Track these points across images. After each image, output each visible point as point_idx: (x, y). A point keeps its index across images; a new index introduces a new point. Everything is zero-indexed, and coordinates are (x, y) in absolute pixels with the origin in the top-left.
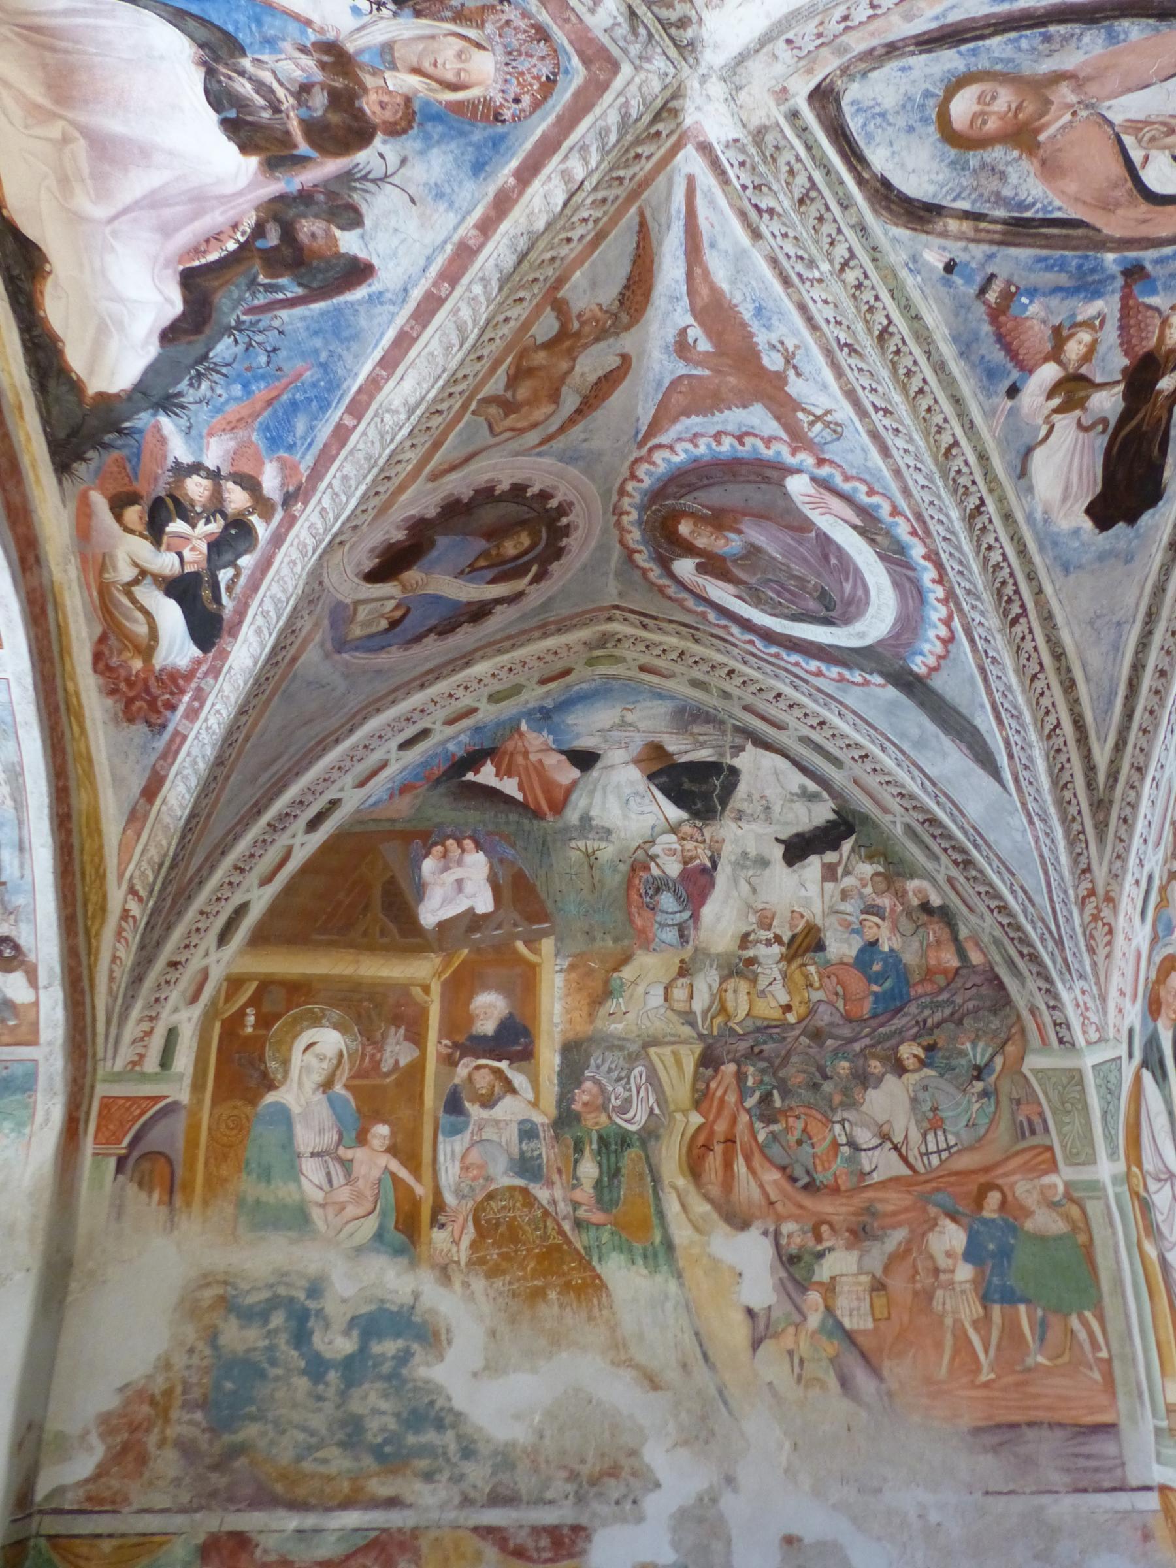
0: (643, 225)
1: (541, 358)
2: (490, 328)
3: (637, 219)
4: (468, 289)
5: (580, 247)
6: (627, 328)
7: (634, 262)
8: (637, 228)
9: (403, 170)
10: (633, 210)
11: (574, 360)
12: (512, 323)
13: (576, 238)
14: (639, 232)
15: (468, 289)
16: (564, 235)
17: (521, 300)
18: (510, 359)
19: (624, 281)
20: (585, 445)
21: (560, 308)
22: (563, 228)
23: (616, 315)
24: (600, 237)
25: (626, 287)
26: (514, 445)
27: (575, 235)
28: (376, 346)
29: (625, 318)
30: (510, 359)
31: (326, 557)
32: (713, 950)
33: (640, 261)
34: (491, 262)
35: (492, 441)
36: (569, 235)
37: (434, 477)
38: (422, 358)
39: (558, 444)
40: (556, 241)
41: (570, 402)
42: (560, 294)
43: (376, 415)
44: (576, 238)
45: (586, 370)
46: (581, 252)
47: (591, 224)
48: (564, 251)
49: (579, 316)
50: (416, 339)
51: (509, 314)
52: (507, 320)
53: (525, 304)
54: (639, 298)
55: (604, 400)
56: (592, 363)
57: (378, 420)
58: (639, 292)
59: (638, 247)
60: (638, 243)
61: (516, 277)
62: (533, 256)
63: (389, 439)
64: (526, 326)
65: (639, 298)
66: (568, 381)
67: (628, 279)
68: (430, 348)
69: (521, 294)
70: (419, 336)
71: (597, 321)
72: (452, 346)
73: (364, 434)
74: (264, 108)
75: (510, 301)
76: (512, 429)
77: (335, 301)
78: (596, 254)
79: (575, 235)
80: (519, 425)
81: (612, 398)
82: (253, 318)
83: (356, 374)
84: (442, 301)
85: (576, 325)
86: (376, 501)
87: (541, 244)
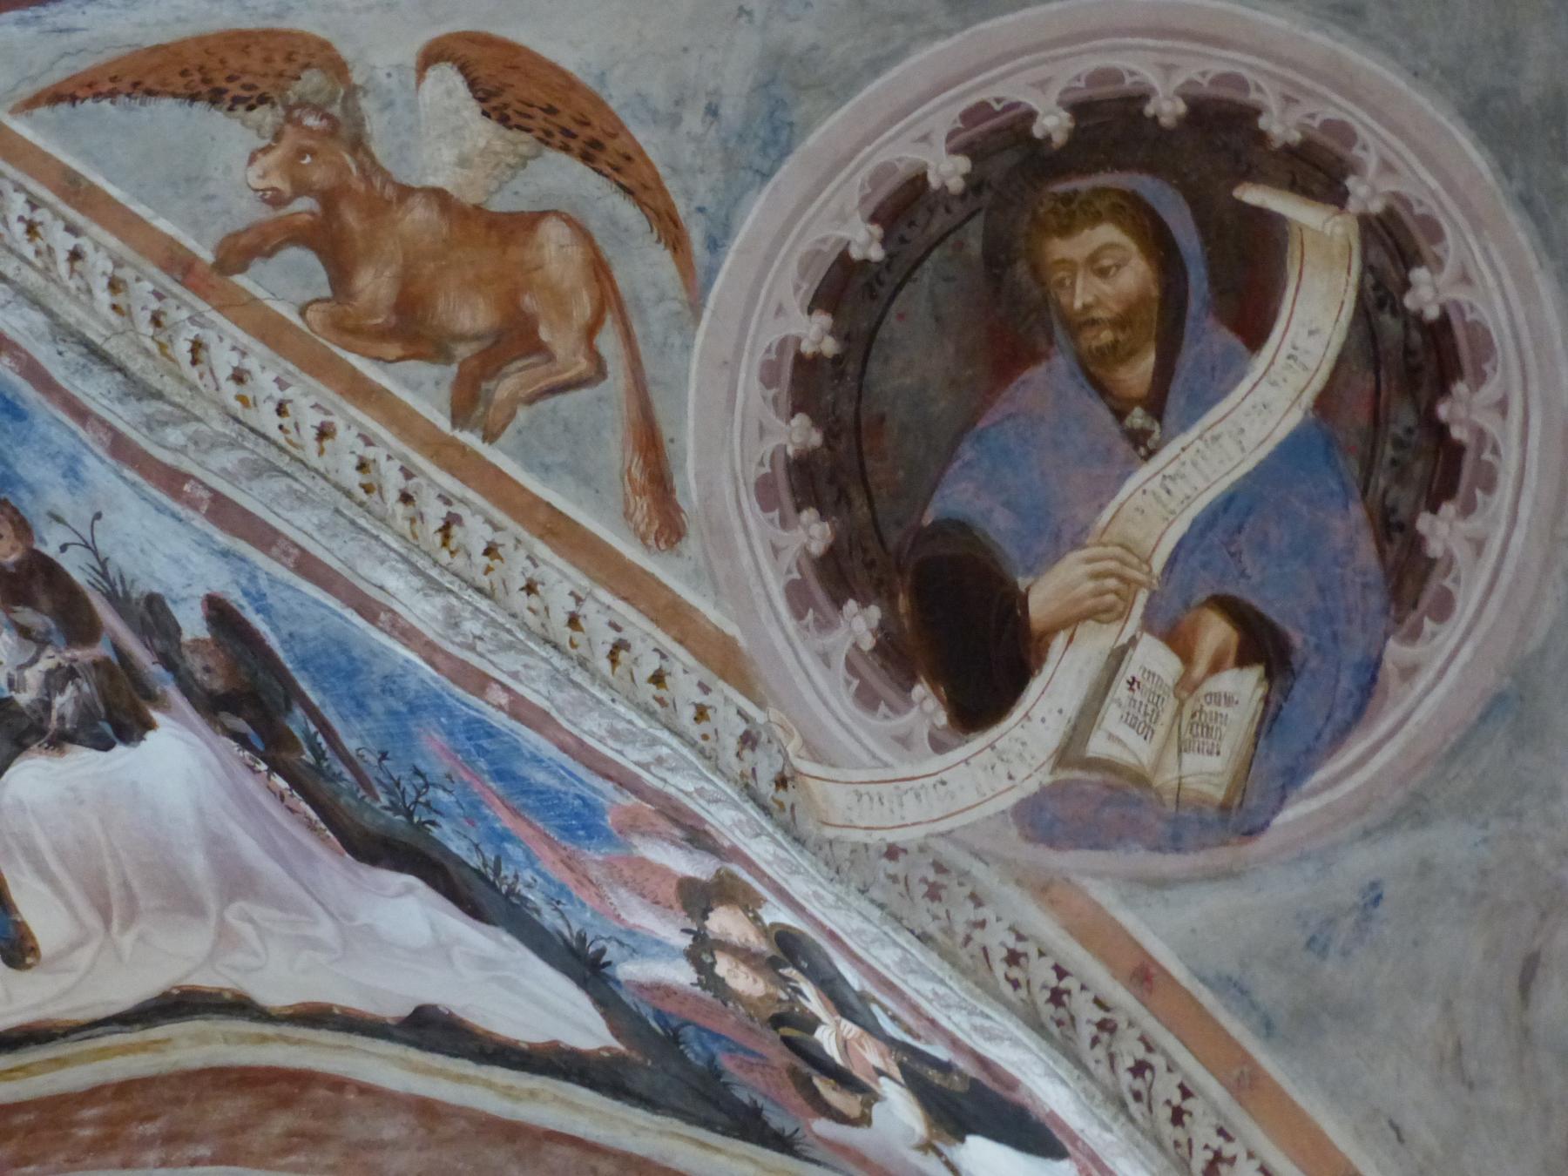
0: (56, 96)
1: (375, 285)
2: (250, 416)
3: (43, 112)
4: (182, 450)
5: (95, 229)
6: (338, 68)
7: (150, 93)
8: (63, 109)
9: (68, 520)
10: (21, 127)
11: (405, 192)
12: (251, 364)
13: (70, 242)
14: (73, 99)
15: (182, 450)
16: (63, 268)
17: (197, 347)
18: (353, 359)
19: (200, 108)
20: (727, 110)
21: (240, 252)
22: (46, 272)
23: (289, 109)
24: (74, 189)
25: (215, 97)
26: (652, 323)
27: (63, 243)
28: (341, 617)
29: (312, 81)
30: (353, 359)
31: (808, 826)
32: (1071, 125)
33: (149, 82)
34: (118, 408)
35: (617, 378)
36: (62, 256)
37: (668, 527)
38: (334, 545)
39: (689, 196)
40: (72, 284)
41: (560, 176)
42: (207, 256)
43: (472, 648)
44: (70, 242)
45: (448, 155)
46: (104, 224)
47: (41, 215)
48: (99, 264)
49: (276, 200)
50: (303, 551)
51: (224, 372)
52: (239, 377)
53: (209, 337)
54: (254, 62)
55: (569, 83)
56: (438, 140)
57: (480, 646)
58: (235, 62)
59: (112, 95)
60: (98, 96)
61: (137, 365)
62: (95, 333)
63: (506, 637)
64: (271, 331)
65: (254, 62)
66: (470, 197)
67: (194, 98)
68: (309, 528)
69: (182, 348)
70: (296, 545)
71: (301, 152)
72: (290, 487)
73: (514, 675)
74: (79, 688)
75: (192, 373)
76: (591, 330)
77: (289, 666)
78: (114, 191)
79: (63, 243)
80: (583, 308)
81: (568, 59)
82: (379, 790)
83: (407, 661)
84: (217, 497)
85: (304, 205)
86: (686, 683)
87: (72, 313)
